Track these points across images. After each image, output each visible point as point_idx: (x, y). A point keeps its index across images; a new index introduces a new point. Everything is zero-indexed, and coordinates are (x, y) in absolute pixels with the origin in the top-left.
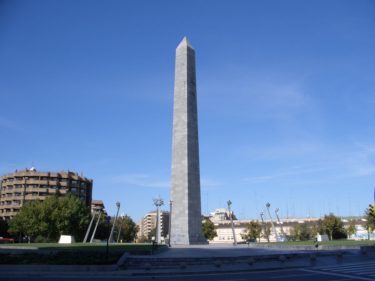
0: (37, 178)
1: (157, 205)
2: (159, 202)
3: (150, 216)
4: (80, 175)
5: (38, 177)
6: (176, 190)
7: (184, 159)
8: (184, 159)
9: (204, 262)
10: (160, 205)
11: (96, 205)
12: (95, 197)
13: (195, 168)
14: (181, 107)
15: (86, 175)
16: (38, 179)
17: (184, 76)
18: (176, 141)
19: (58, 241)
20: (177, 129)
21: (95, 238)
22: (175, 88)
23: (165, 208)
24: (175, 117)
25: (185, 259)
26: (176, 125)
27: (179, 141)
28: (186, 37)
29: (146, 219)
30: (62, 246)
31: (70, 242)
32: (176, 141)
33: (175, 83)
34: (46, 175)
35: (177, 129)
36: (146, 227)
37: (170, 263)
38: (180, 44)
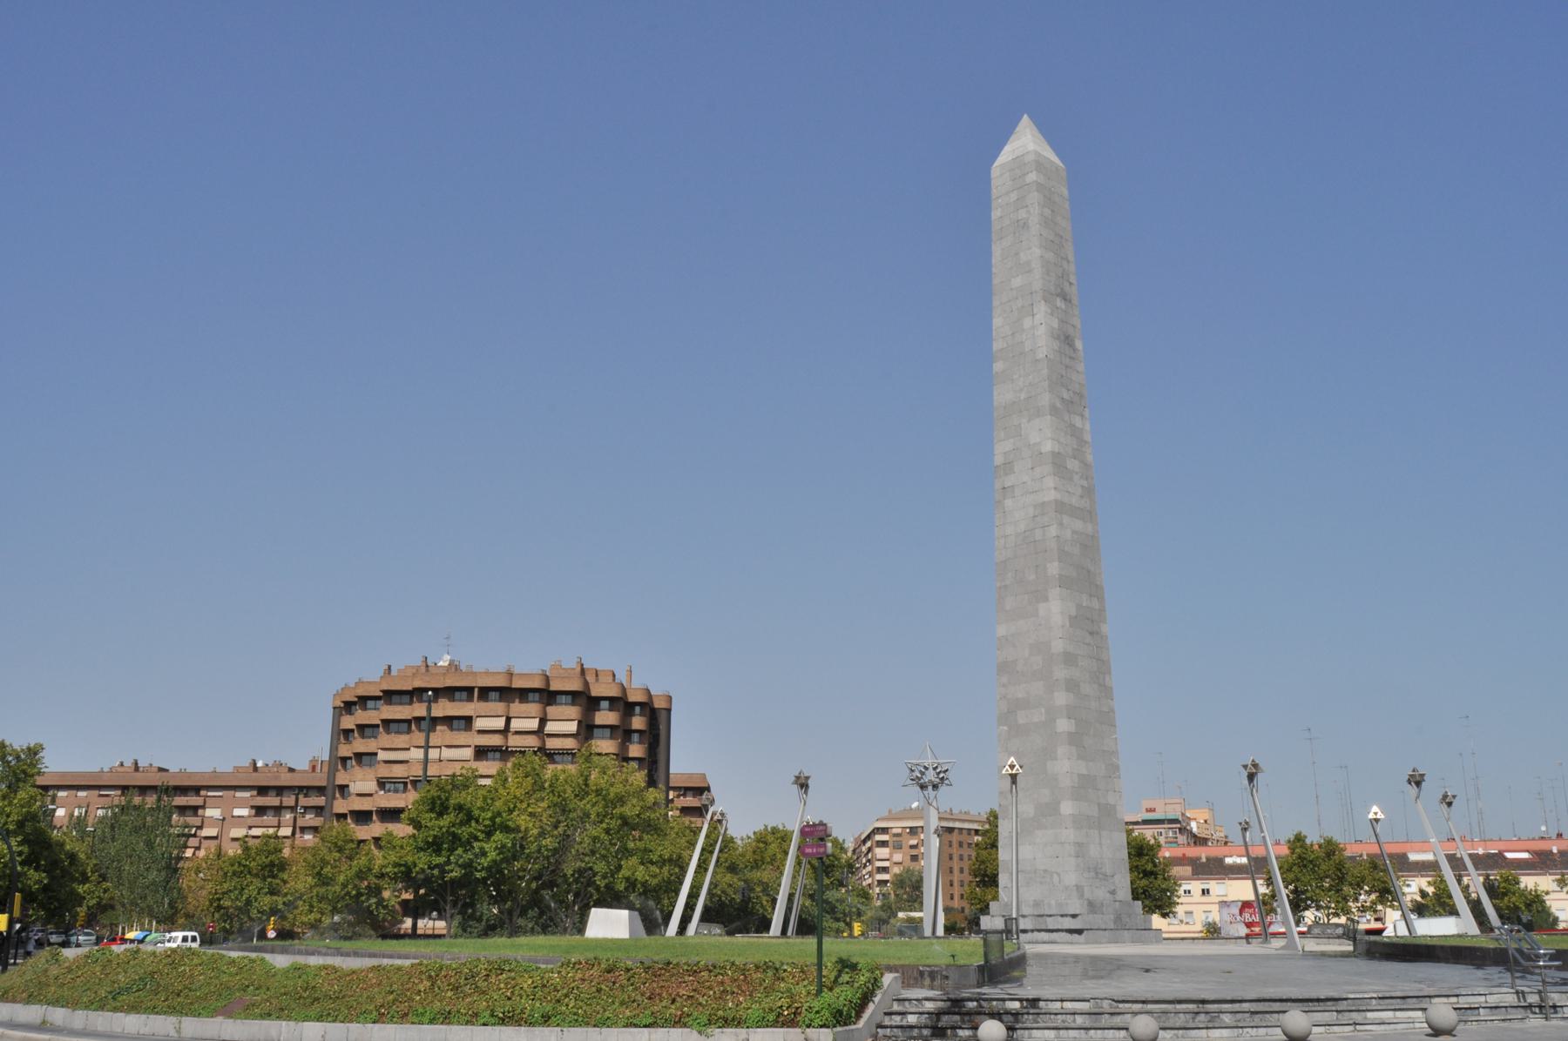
0: (464, 694)
1: (923, 787)
2: (931, 776)
3: (884, 830)
4: (622, 677)
5: (470, 690)
6: (1021, 721)
7: (1046, 599)
8: (1046, 599)
9: (1227, 1019)
10: (935, 787)
11: (686, 791)
12: (682, 762)
13: (1091, 633)
14: (1023, 396)
15: (645, 677)
16: (470, 699)
17: (1030, 271)
18: (1009, 530)
19: (581, 930)
20: (1009, 481)
21: (703, 919)
22: (997, 322)
23: (968, 800)
24: (1002, 435)
25: (1058, 1004)
26: (1008, 467)
27: (1022, 527)
28: (1031, 118)
29: (869, 844)
30: (1423, 942)
31: (627, 936)
32: (1009, 530)
33: (996, 303)
34: (537, 684)
35: (1009, 481)
36: (871, 874)
37: (1079, 1020)
38: (1007, 148)
